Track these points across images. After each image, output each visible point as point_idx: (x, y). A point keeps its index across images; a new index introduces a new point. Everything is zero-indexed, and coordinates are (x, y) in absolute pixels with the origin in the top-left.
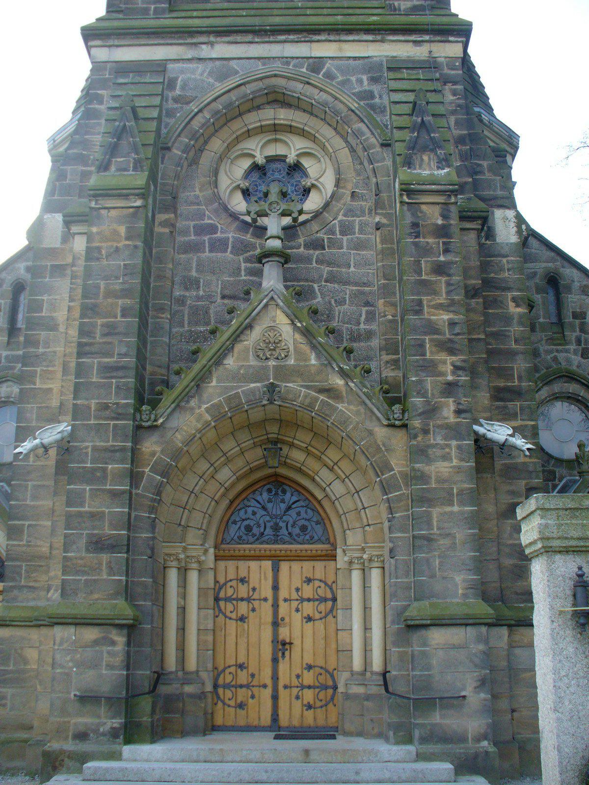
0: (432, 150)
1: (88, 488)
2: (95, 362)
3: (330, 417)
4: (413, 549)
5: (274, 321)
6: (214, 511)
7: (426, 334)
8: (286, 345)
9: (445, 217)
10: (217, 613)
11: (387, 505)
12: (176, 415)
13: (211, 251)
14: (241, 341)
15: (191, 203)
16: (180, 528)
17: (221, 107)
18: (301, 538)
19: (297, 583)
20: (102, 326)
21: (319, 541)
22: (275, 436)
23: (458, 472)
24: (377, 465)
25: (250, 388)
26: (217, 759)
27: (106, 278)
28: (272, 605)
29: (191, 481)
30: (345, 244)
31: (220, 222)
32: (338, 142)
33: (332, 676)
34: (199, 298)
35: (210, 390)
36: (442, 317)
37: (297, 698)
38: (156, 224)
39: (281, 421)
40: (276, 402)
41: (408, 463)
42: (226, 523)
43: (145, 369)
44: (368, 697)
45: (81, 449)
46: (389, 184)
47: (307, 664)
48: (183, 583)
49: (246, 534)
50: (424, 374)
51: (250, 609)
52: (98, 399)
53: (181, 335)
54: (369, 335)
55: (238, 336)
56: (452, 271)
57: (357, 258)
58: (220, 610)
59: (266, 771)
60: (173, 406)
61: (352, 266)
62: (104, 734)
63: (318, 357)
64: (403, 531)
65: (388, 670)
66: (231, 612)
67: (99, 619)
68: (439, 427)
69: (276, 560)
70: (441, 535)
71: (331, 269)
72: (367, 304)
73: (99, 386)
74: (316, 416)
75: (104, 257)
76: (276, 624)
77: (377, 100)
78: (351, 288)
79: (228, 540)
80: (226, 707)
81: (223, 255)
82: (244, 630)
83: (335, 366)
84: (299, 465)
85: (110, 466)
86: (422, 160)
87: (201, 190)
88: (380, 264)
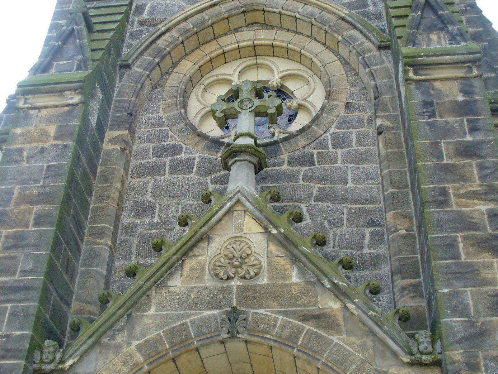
0: (441, 29)
3: (320, 354)
5: (241, 230)
7: (456, 230)
8: (256, 259)
9: (465, 92)
12: (94, 355)
14: (195, 256)
15: (153, 125)
17: (192, 26)
20: (7, 237)
25: (205, 317)
27: (22, 182)
30: (339, 157)
31: (185, 142)
32: (329, 56)
34: (152, 225)
35: (146, 321)
36: (478, 208)
38: (106, 140)
43: (68, 305)
46: (391, 86)
50: (460, 284)
54: (376, 261)
55: (191, 249)
56: (484, 152)
60: (90, 342)
61: (350, 182)
63: (302, 273)
71: (323, 186)
72: (372, 223)
74: (300, 354)
75: (25, 159)
77: (371, 8)
78: (349, 206)
81: (187, 176)
83: (326, 282)
86: (430, 40)
87: (165, 111)
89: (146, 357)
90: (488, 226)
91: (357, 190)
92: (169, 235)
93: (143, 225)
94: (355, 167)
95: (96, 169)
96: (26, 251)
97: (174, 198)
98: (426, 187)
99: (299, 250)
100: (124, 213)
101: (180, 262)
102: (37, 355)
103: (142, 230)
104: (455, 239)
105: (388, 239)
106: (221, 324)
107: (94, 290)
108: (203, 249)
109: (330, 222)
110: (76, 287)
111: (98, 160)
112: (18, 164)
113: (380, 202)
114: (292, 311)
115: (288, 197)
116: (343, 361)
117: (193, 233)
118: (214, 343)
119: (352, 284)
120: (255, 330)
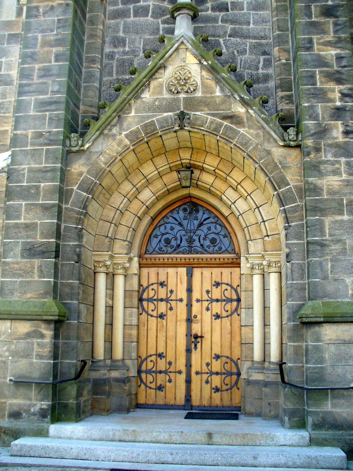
1: (24, 203)
2: (31, 99)
4: (308, 254)
5: (185, 62)
6: (138, 226)
7: (316, 67)
10: (141, 312)
11: (283, 215)
12: (100, 140)
13: (135, 16)
14: (157, 78)
16: (107, 240)
18: (211, 248)
19: (207, 286)
20: (39, 70)
21: (226, 251)
22: (188, 161)
23: (347, 185)
24: (275, 180)
25: (165, 117)
26: (131, 438)
27: (43, 31)
28: (187, 305)
29: (117, 200)
33: (236, 364)
34: (125, 53)
35: (130, 120)
37: (207, 382)
39: (193, 148)
40: (186, 128)
41: (302, 179)
42: (149, 237)
43: (79, 108)
44: (266, 384)
45: (19, 171)
47: (215, 354)
48: (111, 287)
49: (166, 246)
50: (315, 101)
51: (168, 308)
52: (34, 129)
53: (111, 83)
54: (266, 78)
55: (154, 74)
56: (339, 13)
57: (256, 16)
58: (143, 309)
59: (172, 454)
60: (98, 133)
62: (34, 414)
63: (222, 90)
64: (298, 239)
65: (284, 361)
66: (152, 311)
67: (29, 315)
68: (330, 146)
69: (190, 267)
70: (332, 241)
71: (234, 26)
72: (264, 53)
73: (35, 118)
74: (221, 139)
75: (41, 14)
76: (189, 320)
78: (251, 41)
79: (151, 250)
80: (147, 388)
81: (145, 18)
82: (163, 325)
84: (209, 187)
85: (42, 184)
88: (275, 19)
89: (131, 141)
90: (335, 65)
91: (255, 30)
92: (136, 60)
93: (118, 53)
94: (255, 13)
95: (85, 15)
96: (53, 78)
97: (137, 34)
98: (300, 37)
99: (220, 75)
100: (106, 45)
101: (148, 82)
102: (68, 142)
103: (118, 56)
104: (314, 73)
105: (274, 65)
106: (175, 121)
107: (93, 98)
108: (161, 74)
109: (238, 51)
110: (82, 96)
111: (86, 9)
112: (37, 18)
113: (270, 39)
114: (216, 113)
115: (212, 34)
116: (246, 144)
117: (155, 64)
118: (171, 132)
119: (252, 98)
120: (195, 124)
